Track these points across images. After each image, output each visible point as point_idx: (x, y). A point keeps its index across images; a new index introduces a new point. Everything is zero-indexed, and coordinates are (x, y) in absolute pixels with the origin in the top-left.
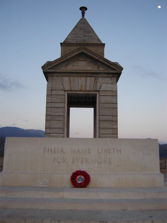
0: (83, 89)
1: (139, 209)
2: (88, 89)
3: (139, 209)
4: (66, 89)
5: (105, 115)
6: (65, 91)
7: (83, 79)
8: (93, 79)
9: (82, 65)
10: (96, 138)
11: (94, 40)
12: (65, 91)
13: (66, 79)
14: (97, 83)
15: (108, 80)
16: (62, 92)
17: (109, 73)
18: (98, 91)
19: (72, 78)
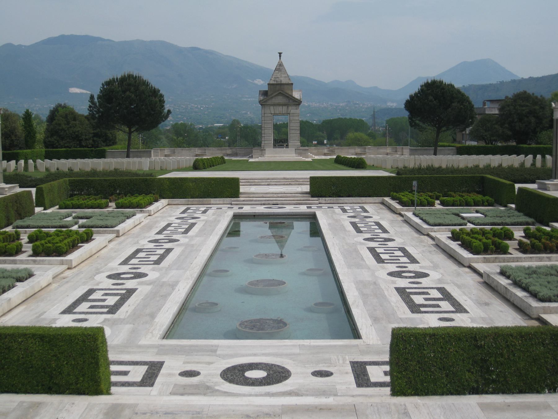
0: (281, 113)
1: (166, 111)
2: (283, 113)
3: (166, 111)
4: (272, 113)
5: (99, 250)
6: (272, 114)
7: (281, 107)
8: (286, 107)
9: (280, 99)
10: (334, 162)
11: (206, 164)
12: (272, 114)
13: (272, 107)
14: (288, 109)
15: (294, 107)
16: (270, 115)
17: (294, 104)
18: (289, 114)
19: (275, 107)
